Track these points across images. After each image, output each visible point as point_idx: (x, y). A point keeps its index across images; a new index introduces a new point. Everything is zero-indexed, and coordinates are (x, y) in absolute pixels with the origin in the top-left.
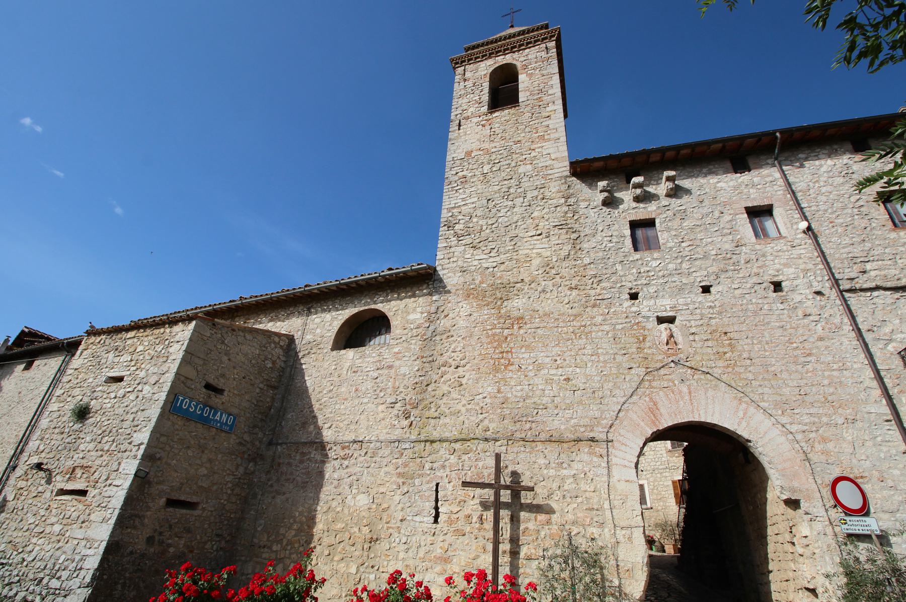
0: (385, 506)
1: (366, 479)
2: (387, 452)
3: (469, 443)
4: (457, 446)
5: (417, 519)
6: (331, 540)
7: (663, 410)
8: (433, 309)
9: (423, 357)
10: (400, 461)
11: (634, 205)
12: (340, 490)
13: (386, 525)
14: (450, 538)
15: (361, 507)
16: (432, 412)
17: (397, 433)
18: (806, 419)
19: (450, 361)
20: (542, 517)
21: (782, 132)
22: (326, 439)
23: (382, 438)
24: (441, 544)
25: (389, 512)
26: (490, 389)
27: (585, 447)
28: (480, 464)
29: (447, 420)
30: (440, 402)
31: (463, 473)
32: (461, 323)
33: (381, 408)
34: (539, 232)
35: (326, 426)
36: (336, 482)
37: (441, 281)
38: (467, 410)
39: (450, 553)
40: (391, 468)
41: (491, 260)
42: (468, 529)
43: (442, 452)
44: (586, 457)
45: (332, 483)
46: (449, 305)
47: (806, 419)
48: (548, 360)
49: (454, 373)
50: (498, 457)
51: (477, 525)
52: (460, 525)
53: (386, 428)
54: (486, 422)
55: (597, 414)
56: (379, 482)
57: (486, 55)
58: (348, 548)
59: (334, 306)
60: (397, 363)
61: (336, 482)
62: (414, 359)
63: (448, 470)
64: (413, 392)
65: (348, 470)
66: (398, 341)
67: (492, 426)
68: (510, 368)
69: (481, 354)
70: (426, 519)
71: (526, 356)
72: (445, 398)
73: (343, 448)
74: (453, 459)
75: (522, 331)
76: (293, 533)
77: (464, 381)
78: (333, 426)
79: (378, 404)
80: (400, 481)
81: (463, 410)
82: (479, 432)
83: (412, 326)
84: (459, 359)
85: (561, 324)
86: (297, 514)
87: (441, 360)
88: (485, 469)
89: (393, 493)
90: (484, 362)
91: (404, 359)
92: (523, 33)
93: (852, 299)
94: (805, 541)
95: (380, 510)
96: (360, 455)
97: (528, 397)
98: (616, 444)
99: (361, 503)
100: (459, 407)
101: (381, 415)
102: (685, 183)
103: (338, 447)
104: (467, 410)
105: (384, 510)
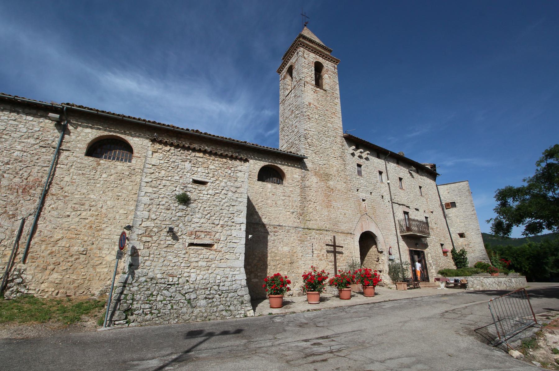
0: (295, 251)
1: (285, 240)
2: (294, 231)
3: (321, 231)
4: (318, 232)
5: (307, 255)
6: (274, 263)
7: (364, 227)
8: (303, 176)
9: (301, 195)
10: (299, 235)
11: (358, 158)
12: (275, 244)
13: (296, 258)
14: (318, 261)
15: (285, 251)
16: (307, 218)
17: (296, 225)
18: (385, 233)
19: (312, 199)
20: (341, 255)
21: (391, 152)
22: (265, 223)
23: (290, 225)
24: (316, 263)
25: (297, 253)
26: (326, 213)
27: (349, 236)
28: (326, 238)
29: (313, 222)
30: (310, 215)
31: (321, 241)
32: (314, 185)
33: (288, 213)
34: (335, 156)
35: (264, 217)
36: (272, 242)
37: (305, 164)
38: (320, 220)
39: (318, 266)
40: (295, 237)
41: (321, 161)
42: (323, 258)
43: (313, 233)
44: (349, 238)
45: (271, 242)
46: (309, 176)
47: (385, 233)
48: (340, 206)
49: (313, 205)
50: (334, 237)
51: (326, 257)
52: (321, 257)
53: (291, 222)
54: (326, 224)
55: (352, 226)
56: (291, 242)
57: (313, 50)
58: (282, 266)
59: (254, 157)
60: (292, 195)
61: (272, 242)
62: (298, 195)
63: (316, 239)
64: (299, 209)
65: (277, 237)
66: (291, 186)
67: (328, 226)
68: (331, 207)
69: (322, 200)
70: (310, 255)
71: (335, 203)
72: (312, 214)
73: (274, 228)
74: (317, 236)
75: (333, 194)
76: (256, 261)
77: (317, 208)
78: (267, 218)
79: (287, 211)
80: (300, 242)
81: (318, 219)
82: (324, 228)
83: (296, 180)
84: (315, 199)
85: (343, 195)
86: (256, 254)
87: (308, 199)
88: (329, 241)
89: (297, 247)
90: (324, 203)
91: (295, 194)
92: (319, 45)
93: (394, 205)
94: (382, 261)
95: (292, 254)
96: (282, 231)
97: (336, 218)
98: (355, 235)
99: (285, 250)
100: (317, 218)
101: (288, 217)
102: (369, 157)
103: (272, 227)
104: (320, 220)
105: (295, 252)
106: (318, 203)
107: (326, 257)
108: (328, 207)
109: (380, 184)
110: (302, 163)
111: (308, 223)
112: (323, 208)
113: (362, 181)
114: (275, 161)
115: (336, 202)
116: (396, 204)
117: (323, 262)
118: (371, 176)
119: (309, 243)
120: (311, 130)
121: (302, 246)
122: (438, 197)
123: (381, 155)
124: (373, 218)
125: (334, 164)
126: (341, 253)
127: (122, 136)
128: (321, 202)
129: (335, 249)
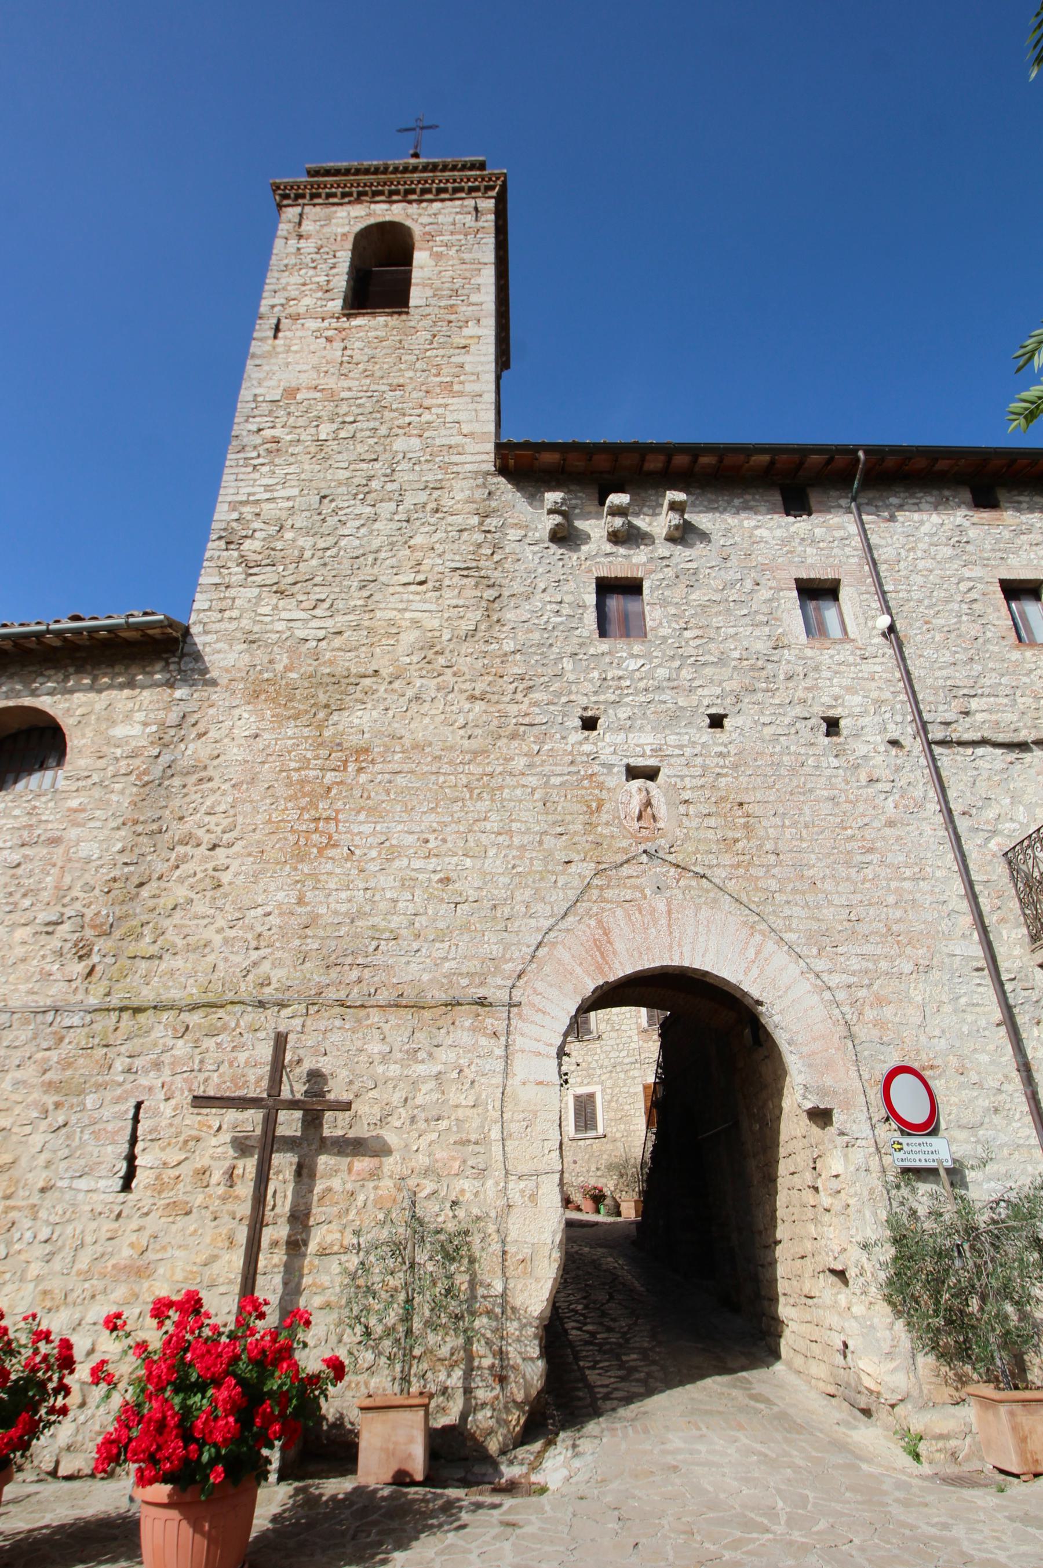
3: (221, 1012)
4: (194, 1019)
7: (619, 945)
9: (136, 822)
11: (609, 547)
17: (55, 992)
19: (200, 833)
20: (363, 1164)
21: (869, 451)
28: (242, 1057)
34: (421, 577)
38: (226, 941)
43: (158, 1032)
44: (464, 1037)
47: (855, 964)
48: (410, 839)
51: (221, 1190)
54: (265, 967)
55: (496, 951)
64: (103, 899)
67: (278, 975)
70: (102, 1184)
80: (50, 1100)
81: (217, 939)
83: (118, 752)
87: (178, 830)
93: (945, 756)
98: (525, 1010)
102: (702, 520)
106: (237, 847)
107: (221, 1190)
108: (301, 857)
109: (809, 653)
110: (183, 655)
111: (142, 972)
112: (263, 871)
113: (633, 664)
114: (27, 684)
115: (374, 812)
116: (980, 751)
117: (191, 1223)
118: (716, 621)
119: (117, 1101)
120: (276, 494)
121: (61, 1121)
122: (915, 672)
123: (814, 499)
124: (719, 875)
125: (408, 615)
126: (568, 1055)
127: (27, 701)
128: (257, 836)
129: (290, 1144)
